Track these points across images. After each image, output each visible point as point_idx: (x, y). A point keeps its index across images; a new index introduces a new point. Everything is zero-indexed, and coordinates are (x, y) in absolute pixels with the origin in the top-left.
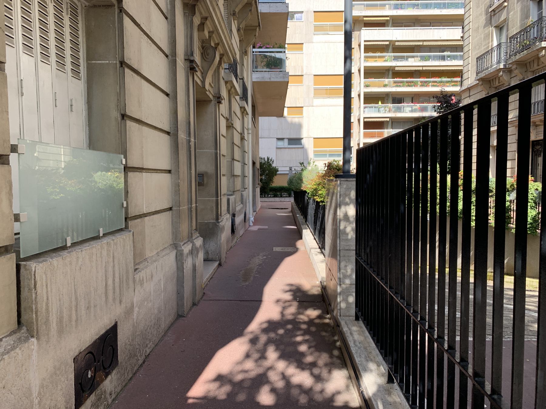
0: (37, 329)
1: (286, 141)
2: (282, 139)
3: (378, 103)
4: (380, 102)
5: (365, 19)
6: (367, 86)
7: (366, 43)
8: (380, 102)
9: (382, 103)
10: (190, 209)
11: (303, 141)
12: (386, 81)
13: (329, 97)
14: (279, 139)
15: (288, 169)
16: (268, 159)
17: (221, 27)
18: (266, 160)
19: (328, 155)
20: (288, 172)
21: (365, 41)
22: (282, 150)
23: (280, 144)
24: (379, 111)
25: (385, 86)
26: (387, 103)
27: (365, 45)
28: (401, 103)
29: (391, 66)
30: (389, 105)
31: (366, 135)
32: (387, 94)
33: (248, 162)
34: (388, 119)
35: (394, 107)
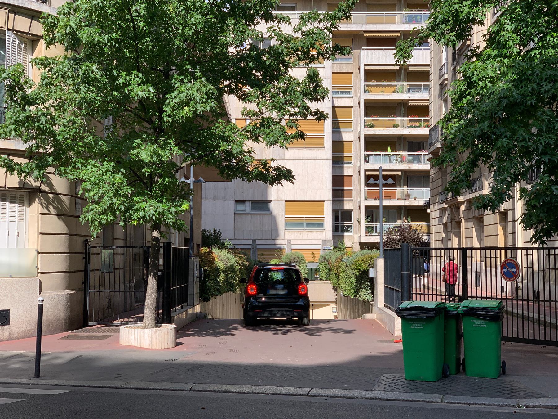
0: (421, 49)
1: (248, 205)
2: (243, 202)
3: (386, 151)
4: (389, 149)
5: (366, 34)
6: (369, 126)
7: (368, 68)
8: (389, 149)
9: (392, 151)
10: (130, 270)
11: (272, 206)
12: (398, 120)
13: (306, 148)
14: (238, 202)
15: (250, 242)
16: (215, 231)
17: (130, 262)
18: (212, 232)
19: (305, 224)
20: (250, 247)
21: (366, 65)
22: (244, 216)
23: (240, 208)
24: (390, 162)
25: (396, 126)
26: (399, 151)
27: (365, 70)
28: (419, 150)
29: (403, 100)
30: (401, 153)
31: (369, 195)
32: (400, 138)
33: (175, 242)
34: (400, 173)
35: (409, 155)
